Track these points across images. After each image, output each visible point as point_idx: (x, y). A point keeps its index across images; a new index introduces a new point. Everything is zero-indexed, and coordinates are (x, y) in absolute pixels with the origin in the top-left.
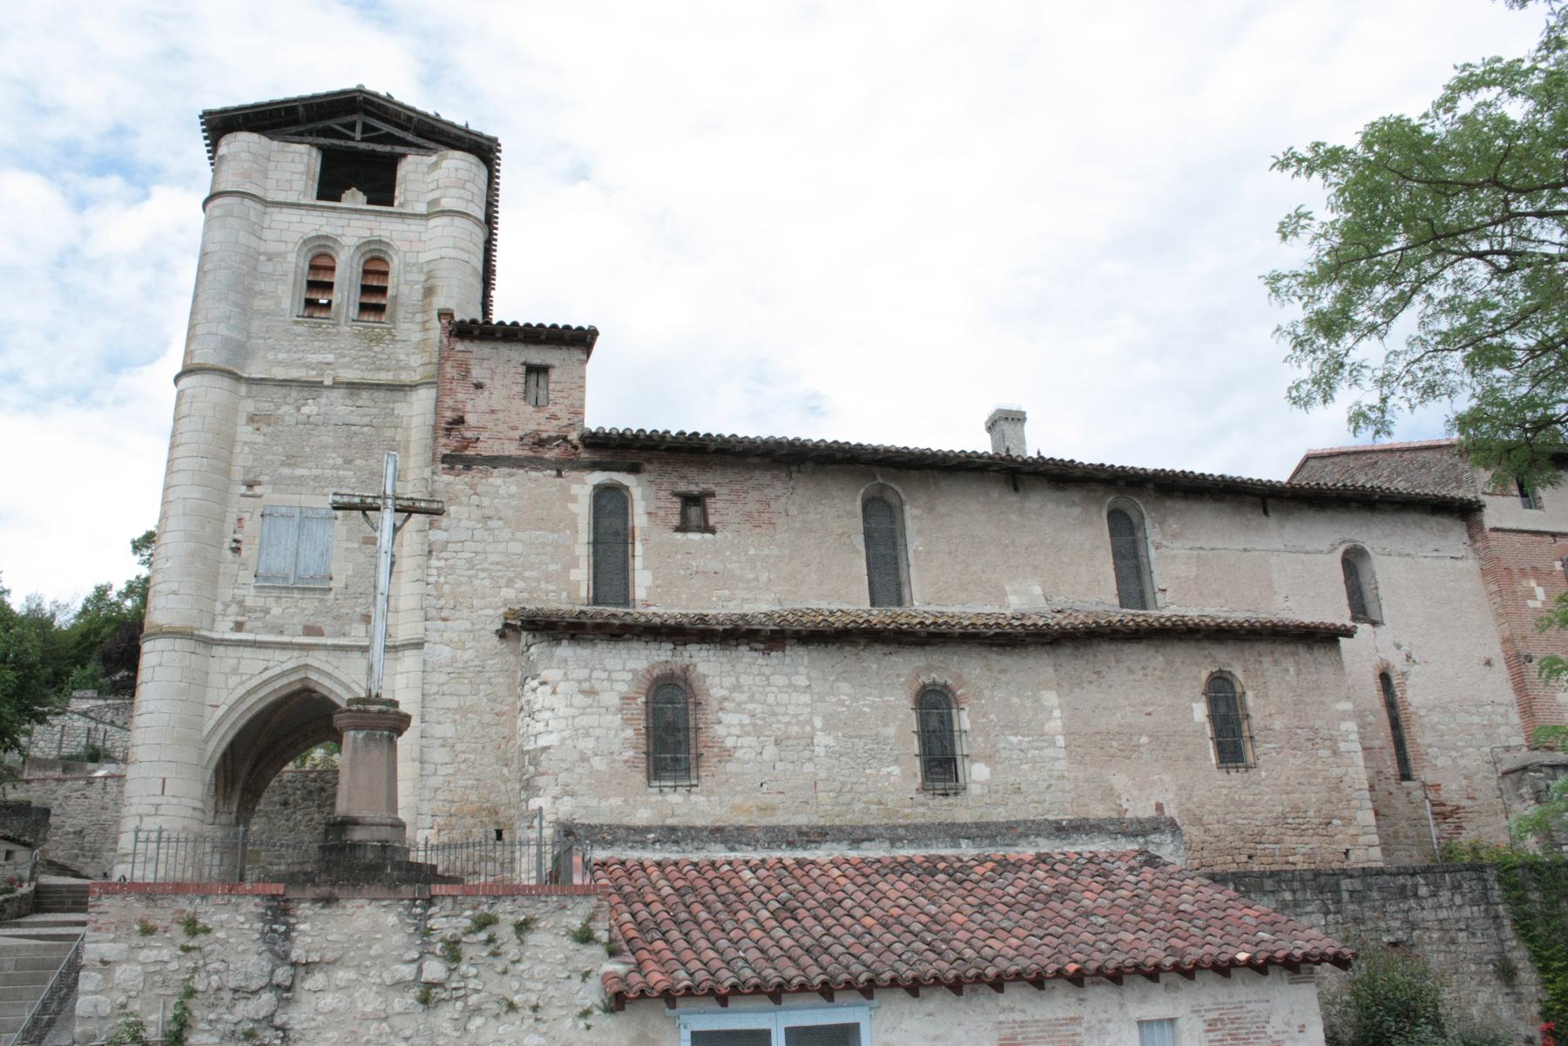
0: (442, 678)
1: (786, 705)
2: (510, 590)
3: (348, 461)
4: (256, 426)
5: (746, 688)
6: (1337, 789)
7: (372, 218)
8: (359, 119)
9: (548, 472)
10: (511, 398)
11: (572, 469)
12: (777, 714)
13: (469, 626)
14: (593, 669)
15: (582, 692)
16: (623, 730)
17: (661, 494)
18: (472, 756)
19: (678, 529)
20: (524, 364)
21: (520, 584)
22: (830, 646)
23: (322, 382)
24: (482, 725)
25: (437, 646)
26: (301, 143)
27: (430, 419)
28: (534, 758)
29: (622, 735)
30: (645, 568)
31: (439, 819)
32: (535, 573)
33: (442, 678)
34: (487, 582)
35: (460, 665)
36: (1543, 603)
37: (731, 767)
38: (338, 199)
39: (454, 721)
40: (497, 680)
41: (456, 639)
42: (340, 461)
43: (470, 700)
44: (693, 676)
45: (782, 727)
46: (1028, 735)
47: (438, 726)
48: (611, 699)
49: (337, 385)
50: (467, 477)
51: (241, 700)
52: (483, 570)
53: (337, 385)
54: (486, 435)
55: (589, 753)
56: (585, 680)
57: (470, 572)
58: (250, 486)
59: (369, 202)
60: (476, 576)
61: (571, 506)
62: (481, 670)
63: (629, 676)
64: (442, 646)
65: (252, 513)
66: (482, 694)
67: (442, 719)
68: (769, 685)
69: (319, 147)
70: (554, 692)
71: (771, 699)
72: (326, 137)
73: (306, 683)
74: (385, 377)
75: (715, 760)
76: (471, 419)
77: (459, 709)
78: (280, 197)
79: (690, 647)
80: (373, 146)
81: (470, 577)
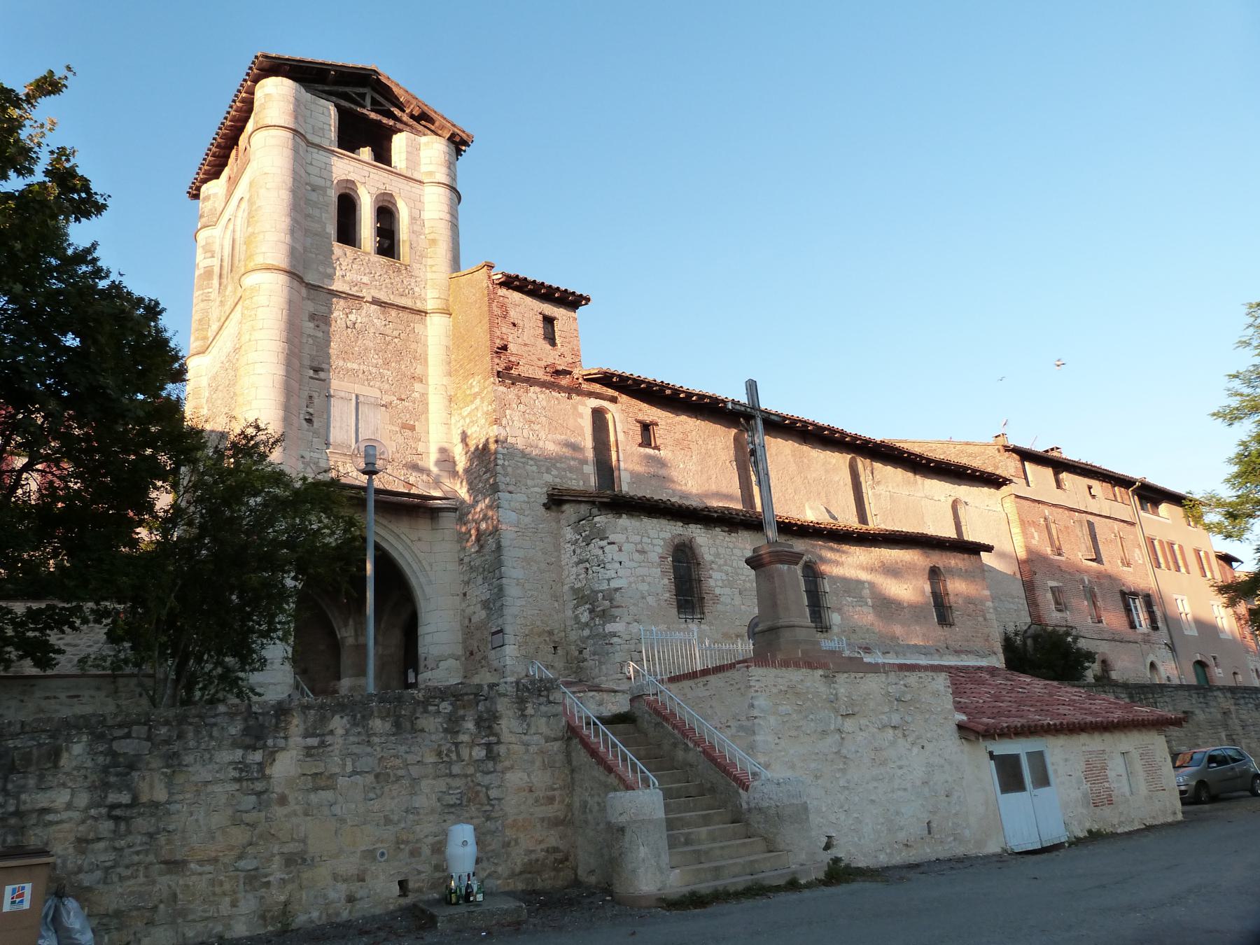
3: (387, 363)
4: (316, 323)
5: (722, 556)
6: (987, 640)
9: (563, 395)
10: (536, 337)
14: (642, 536)
18: (536, 593)
19: (640, 445)
21: (554, 472)
23: (363, 298)
28: (610, 595)
31: (518, 638)
34: (534, 468)
36: (1039, 541)
37: (720, 607)
38: (353, 151)
39: (523, 567)
42: (380, 361)
44: (695, 546)
46: (855, 597)
47: (512, 569)
48: (654, 558)
49: (376, 302)
53: (376, 302)
54: (524, 361)
57: (523, 460)
61: (579, 420)
63: (662, 543)
65: (320, 393)
67: (515, 565)
69: (337, 106)
71: (735, 564)
75: (711, 602)
76: (511, 346)
79: (690, 525)
80: (379, 117)
81: (523, 463)
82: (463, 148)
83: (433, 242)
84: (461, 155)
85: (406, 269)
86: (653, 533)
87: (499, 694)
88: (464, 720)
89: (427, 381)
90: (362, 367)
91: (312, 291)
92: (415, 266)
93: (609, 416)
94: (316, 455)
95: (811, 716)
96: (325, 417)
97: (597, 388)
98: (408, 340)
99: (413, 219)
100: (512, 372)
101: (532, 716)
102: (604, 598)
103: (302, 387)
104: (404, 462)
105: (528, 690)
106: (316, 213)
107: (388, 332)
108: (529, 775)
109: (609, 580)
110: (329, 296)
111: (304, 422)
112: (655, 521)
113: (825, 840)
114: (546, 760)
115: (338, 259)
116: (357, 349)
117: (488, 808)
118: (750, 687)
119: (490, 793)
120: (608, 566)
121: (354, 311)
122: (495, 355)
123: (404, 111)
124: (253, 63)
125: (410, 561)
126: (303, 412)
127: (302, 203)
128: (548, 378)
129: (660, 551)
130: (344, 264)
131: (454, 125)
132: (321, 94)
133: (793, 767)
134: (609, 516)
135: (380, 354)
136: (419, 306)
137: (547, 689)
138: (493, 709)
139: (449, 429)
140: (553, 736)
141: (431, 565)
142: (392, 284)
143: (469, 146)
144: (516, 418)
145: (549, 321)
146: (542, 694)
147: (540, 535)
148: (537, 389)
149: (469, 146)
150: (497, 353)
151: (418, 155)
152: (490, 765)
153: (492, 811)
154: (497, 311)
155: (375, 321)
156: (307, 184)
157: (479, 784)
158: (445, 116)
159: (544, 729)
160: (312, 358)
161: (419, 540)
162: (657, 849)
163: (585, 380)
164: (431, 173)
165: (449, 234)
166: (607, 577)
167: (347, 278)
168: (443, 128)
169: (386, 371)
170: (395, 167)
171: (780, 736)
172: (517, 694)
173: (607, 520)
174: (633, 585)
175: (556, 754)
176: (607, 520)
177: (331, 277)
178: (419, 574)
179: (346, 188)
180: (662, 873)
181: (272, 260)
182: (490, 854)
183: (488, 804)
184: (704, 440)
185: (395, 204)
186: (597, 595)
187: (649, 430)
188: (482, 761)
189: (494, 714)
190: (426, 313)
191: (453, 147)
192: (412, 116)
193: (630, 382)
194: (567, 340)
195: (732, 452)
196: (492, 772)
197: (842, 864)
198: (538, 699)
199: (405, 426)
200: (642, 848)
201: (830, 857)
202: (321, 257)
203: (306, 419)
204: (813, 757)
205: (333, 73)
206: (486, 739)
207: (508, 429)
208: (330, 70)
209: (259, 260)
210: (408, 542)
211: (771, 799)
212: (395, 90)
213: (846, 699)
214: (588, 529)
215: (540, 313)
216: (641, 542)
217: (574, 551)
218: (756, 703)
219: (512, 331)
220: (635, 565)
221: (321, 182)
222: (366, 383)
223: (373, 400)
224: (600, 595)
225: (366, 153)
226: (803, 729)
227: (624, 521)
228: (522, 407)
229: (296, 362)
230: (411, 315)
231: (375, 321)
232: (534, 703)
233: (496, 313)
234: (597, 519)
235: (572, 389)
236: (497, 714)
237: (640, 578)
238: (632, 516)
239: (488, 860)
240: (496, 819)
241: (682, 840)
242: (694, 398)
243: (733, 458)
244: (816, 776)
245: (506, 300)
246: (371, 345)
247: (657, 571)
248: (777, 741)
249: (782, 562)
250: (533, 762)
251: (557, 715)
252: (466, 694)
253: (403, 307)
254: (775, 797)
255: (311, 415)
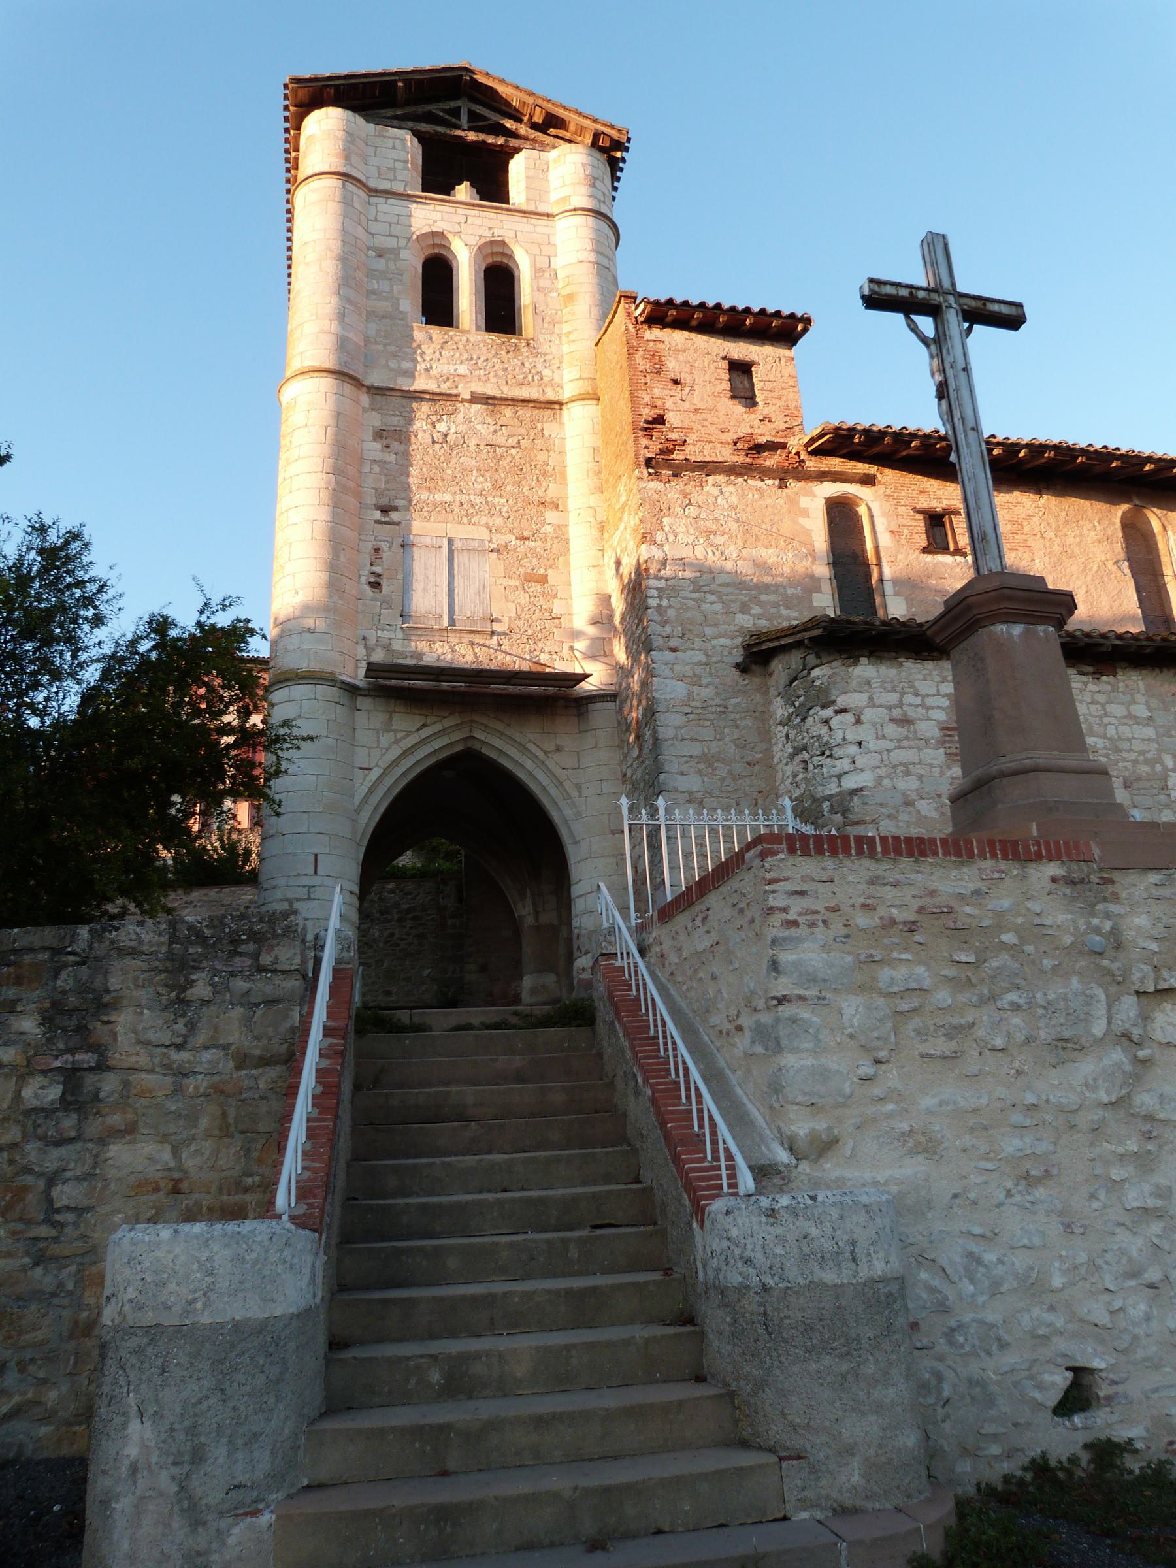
0: (680, 720)
1: (1129, 740)
2: (746, 617)
3: (498, 487)
7: (493, 215)
8: (464, 105)
9: (770, 482)
11: (798, 480)
12: (1121, 751)
13: (703, 659)
14: (903, 693)
15: (892, 720)
16: (949, 767)
17: (901, 510)
19: (925, 550)
20: (724, 358)
21: (756, 610)
22: (1165, 670)
23: (457, 395)
24: (736, 778)
25: (668, 681)
26: (401, 128)
27: (628, 417)
29: (949, 773)
30: (896, 594)
32: (772, 598)
33: (680, 720)
34: (718, 607)
35: (698, 704)
39: (700, 772)
40: (744, 723)
41: (690, 673)
43: (714, 747)
45: (1129, 765)
47: (679, 777)
48: (929, 728)
49: (476, 399)
50: (677, 485)
51: (396, 762)
52: (712, 592)
53: (476, 399)
54: (694, 437)
55: (914, 796)
56: (896, 706)
57: (696, 595)
58: (385, 511)
59: (481, 199)
60: (704, 600)
61: (802, 521)
62: (724, 710)
64: (674, 682)
66: (727, 739)
67: (684, 768)
68: (1106, 715)
69: (416, 133)
70: (858, 721)
71: (1111, 731)
72: (427, 122)
73: (470, 745)
74: (532, 393)
76: (670, 417)
77: (705, 758)
78: (385, 185)
82: (618, 154)
83: (570, 298)
84: (621, 170)
85: (528, 345)
86: (925, 687)
87: (120, 950)
88: (13, 1012)
89: (566, 506)
90: (458, 497)
91: (378, 397)
92: (542, 338)
93: (862, 510)
94: (386, 634)
95: (1013, 996)
96: (400, 576)
97: (834, 463)
98: (532, 449)
99: (538, 271)
100: (674, 456)
101: (204, 1003)
102: (833, 810)
103: (361, 537)
104: (530, 633)
105: (202, 939)
106: (385, 286)
107: (500, 440)
108: (175, 1151)
109: (839, 777)
110: (404, 401)
111: (368, 588)
112: (929, 665)
113: (1061, 1380)
114: (232, 1113)
115: (419, 346)
116: (449, 472)
117: (44, 1231)
118: (771, 911)
119: (55, 1192)
120: (837, 752)
121: (444, 417)
122: (641, 433)
123: (520, 121)
124: (286, 97)
125: (545, 784)
126: (366, 573)
127: (359, 275)
128: (741, 459)
129: (941, 716)
130: (429, 352)
131: (595, 121)
132: (389, 122)
133: (929, 1147)
134: (835, 664)
135: (488, 475)
136: (550, 395)
137: (257, 938)
138: (98, 982)
139: (601, 573)
140: (257, 1052)
141: (579, 787)
142: (505, 370)
143: (627, 149)
144: (683, 529)
145: (740, 369)
146: (243, 948)
147: (732, 717)
148: (720, 478)
149: (627, 149)
150: (646, 429)
151: (546, 179)
152: (69, 1122)
153: (56, 1240)
154: (642, 363)
155: (479, 427)
156: (368, 249)
157: (28, 1170)
158: (580, 110)
159: (235, 1035)
160: (379, 493)
161: (559, 749)
162: (192, 1431)
163: (811, 453)
164: (565, 199)
165: (595, 280)
166: (836, 771)
167: (434, 372)
168: (581, 130)
169: (497, 500)
170: (514, 204)
171: (882, 1054)
172: (170, 951)
173: (831, 672)
174: (886, 782)
175: (264, 1098)
176: (831, 672)
177: (411, 374)
178: (561, 803)
179: (434, 245)
180: (196, 1523)
181: (310, 362)
182: (28, 1354)
183: (48, 1221)
184: (1058, 530)
185: (511, 257)
186: (820, 805)
187: (943, 525)
188: (47, 1112)
189: (98, 998)
190: (561, 404)
191: (602, 158)
192: (534, 126)
193: (887, 440)
194: (776, 394)
195: (1119, 545)
196: (71, 1140)
197: (1135, 1465)
198: (227, 962)
199: (529, 578)
200: (134, 1426)
201: (1083, 1437)
202: (392, 348)
203: (370, 583)
204: (1017, 1117)
205: (400, 84)
206: (68, 1057)
207: (666, 548)
208: (396, 81)
209: (295, 364)
210: (541, 755)
211: (748, 1261)
212: (502, 90)
213: (1154, 946)
214: (801, 692)
215: (724, 358)
216: (900, 704)
217: (787, 737)
218: (786, 957)
219: (672, 393)
220: (891, 745)
221: (391, 243)
222: (465, 520)
223: (476, 544)
224: (826, 805)
225: (463, 191)
226: (980, 1033)
227: (865, 670)
228: (692, 511)
229: (351, 502)
230: (537, 411)
231: (479, 427)
232: (215, 972)
233: (641, 368)
234: (816, 672)
235: (787, 472)
236: (106, 999)
237: (901, 768)
238: (881, 659)
239: (22, 1367)
240: (60, 1261)
241: (435, 1377)
242: (1022, 454)
243: (1122, 556)
244: (1027, 1176)
245: (660, 345)
246: (473, 462)
247: (938, 755)
248: (867, 1069)
249: (1010, 617)
250: (192, 1118)
251: (278, 1001)
252: (31, 950)
253: (524, 401)
254: (759, 1258)
255: (379, 575)
